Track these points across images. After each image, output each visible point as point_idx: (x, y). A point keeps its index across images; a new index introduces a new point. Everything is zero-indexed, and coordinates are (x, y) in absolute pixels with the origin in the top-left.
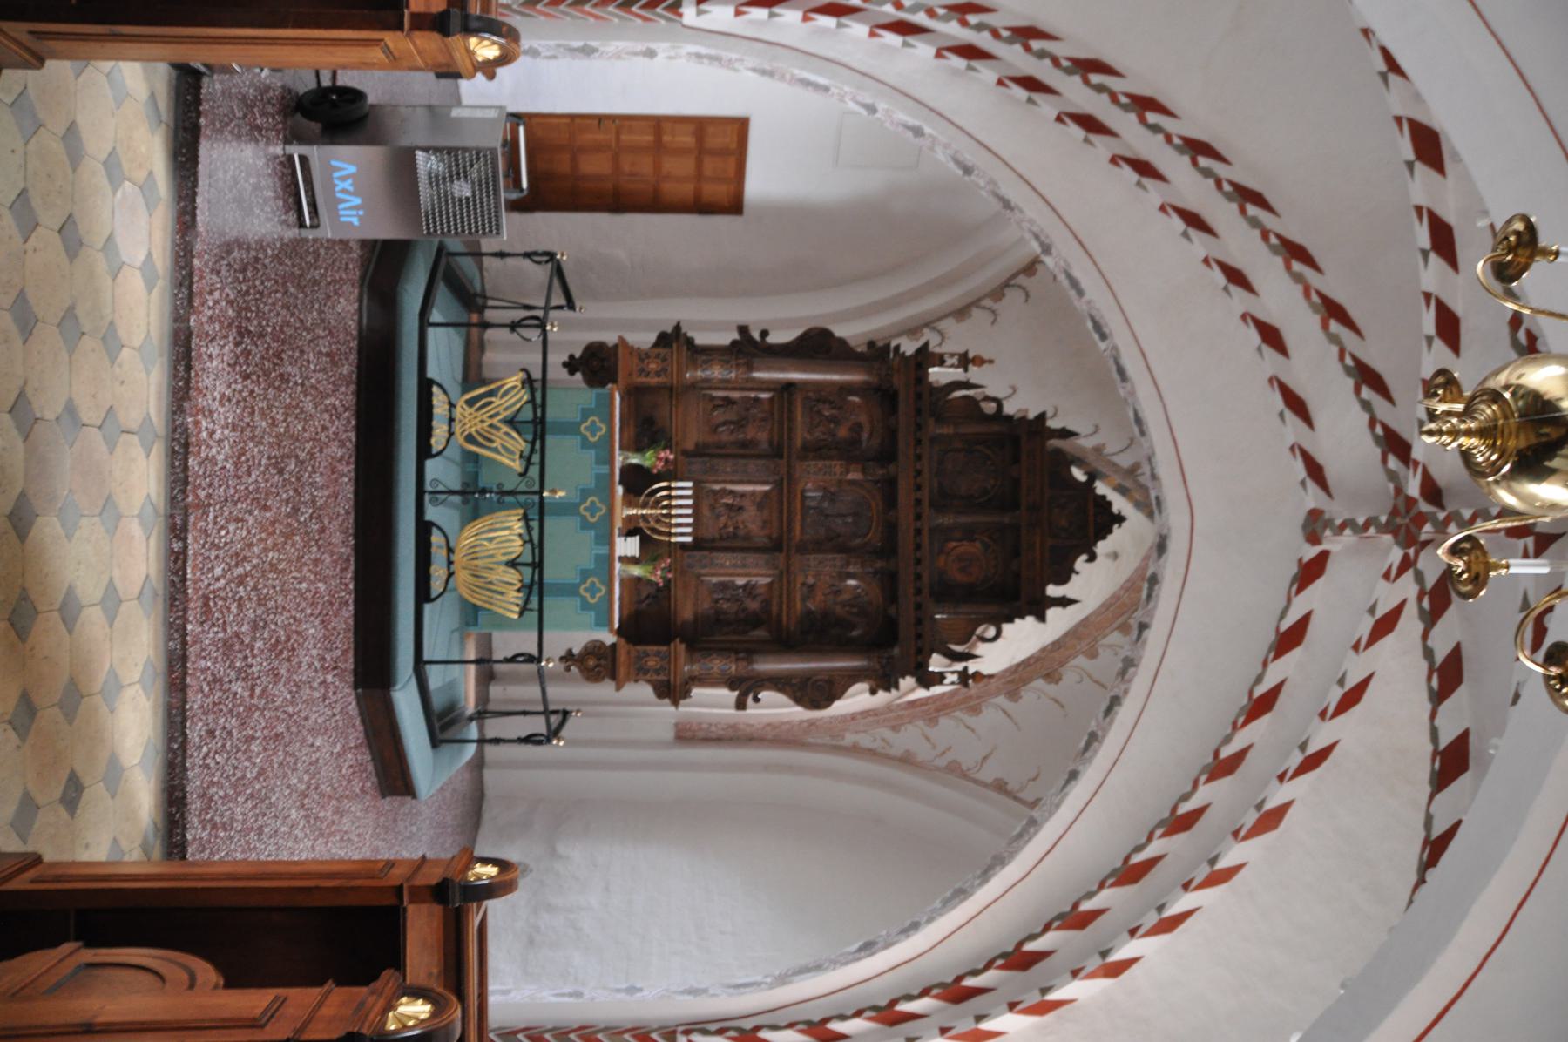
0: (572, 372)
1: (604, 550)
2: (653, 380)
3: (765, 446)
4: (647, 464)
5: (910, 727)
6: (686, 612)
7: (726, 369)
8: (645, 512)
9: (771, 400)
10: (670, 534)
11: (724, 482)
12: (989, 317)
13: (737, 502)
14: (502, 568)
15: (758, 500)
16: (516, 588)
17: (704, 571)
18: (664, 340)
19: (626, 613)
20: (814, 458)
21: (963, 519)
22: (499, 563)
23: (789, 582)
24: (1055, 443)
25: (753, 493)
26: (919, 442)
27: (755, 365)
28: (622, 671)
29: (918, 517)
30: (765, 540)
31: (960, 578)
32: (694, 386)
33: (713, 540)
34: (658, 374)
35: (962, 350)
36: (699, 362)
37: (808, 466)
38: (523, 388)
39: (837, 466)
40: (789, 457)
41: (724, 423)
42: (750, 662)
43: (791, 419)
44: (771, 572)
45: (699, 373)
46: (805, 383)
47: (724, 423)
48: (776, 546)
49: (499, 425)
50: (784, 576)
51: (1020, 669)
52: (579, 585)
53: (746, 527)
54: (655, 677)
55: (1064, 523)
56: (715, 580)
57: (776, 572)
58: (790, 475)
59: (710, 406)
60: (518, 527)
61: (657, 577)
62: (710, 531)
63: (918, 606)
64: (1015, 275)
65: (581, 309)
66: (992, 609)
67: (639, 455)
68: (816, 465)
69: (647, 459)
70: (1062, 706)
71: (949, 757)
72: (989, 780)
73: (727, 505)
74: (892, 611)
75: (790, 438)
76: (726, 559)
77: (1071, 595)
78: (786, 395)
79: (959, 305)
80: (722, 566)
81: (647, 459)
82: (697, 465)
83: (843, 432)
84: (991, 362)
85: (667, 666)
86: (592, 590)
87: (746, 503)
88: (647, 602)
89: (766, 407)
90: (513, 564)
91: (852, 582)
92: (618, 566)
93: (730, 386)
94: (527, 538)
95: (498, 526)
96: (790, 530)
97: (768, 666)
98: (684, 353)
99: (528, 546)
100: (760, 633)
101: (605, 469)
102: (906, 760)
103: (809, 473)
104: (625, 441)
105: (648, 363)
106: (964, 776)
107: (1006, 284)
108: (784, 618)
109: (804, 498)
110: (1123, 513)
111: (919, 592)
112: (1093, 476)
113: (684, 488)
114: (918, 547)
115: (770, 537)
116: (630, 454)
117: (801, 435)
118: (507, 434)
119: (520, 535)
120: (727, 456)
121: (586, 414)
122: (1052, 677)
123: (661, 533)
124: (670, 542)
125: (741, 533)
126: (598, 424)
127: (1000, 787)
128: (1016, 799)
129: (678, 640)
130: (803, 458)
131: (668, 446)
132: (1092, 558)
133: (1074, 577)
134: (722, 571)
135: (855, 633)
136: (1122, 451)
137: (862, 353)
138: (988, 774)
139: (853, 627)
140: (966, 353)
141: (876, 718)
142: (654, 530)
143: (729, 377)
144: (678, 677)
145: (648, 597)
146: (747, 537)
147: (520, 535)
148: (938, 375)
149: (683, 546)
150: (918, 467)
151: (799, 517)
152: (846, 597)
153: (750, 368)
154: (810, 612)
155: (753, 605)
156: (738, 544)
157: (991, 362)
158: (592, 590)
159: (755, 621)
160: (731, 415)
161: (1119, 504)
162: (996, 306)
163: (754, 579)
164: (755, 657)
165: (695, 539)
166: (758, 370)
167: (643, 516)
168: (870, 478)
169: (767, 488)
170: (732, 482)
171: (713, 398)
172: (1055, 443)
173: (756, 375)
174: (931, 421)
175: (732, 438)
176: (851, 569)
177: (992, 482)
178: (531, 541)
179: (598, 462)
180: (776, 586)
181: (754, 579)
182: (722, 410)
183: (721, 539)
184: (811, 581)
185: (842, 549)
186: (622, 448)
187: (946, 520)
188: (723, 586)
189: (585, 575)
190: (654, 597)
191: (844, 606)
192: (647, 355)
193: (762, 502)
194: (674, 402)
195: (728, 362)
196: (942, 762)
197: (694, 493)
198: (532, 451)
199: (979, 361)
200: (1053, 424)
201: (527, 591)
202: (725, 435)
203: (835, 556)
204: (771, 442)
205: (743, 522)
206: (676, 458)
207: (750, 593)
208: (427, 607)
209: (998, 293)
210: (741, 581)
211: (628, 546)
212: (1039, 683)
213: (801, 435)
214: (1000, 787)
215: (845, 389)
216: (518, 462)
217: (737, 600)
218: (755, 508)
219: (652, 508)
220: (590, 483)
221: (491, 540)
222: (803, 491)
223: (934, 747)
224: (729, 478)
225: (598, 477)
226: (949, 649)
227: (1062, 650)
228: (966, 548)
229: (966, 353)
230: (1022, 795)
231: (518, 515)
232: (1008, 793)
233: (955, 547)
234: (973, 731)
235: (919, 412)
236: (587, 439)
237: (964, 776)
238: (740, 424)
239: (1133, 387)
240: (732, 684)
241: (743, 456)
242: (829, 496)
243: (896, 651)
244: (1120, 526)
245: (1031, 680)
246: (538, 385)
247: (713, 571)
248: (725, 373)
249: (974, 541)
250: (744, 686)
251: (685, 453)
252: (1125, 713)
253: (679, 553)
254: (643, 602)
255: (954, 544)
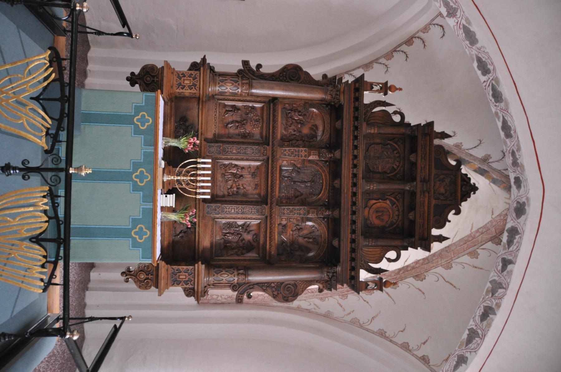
0: (133, 85)
1: (149, 206)
2: (187, 92)
3: (258, 136)
4: (181, 146)
5: (331, 299)
6: (205, 241)
7: (235, 86)
8: (179, 178)
9: (262, 108)
10: (196, 193)
11: (232, 159)
12: (383, 69)
13: (240, 172)
14: (27, 243)
15: (253, 171)
16: (41, 263)
17: (217, 216)
18: (194, 66)
19: (166, 243)
20: (288, 146)
21: (382, 187)
22: (23, 240)
23: (271, 224)
24: (437, 142)
25: (249, 167)
26: (356, 138)
27: (254, 85)
28: (162, 283)
29: (355, 185)
30: (256, 196)
31: (376, 222)
32: (212, 97)
33: (224, 196)
34: (190, 88)
35: (384, 82)
36: (218, 81)
37: (285, 150)
38: (50, 66)
39: (303, 151)
40: (273, 144)
41: (232, 122)
42: (246, 275)
43: (275, 121)
44: (259, 217)
45: (218, 89)
46: (284, 98)
47: (232, 122)
48: (263, 201)
49: (24, 101)
50: (268, 220)
51: (401, 272)
52: (131, 230)
53: (244, 188)
54: (185, 286)
55: (442, 190)
56: (224, 221)
57: (263, 217)
58: (273, 156)
59: (224, 110)
60: (43, 204)
61: (187, 221)
62: (222, 190)
63: (353, 241)
64: (400, 45)
65: (136, 36)
66: (397, 243)
67: (176, 141)
68: (289, 150)
69: (182, 143)
70: (423, 293)
71: (352, 316)
72: (375, 329)
73: (233, 174)
74: (335, 243)
75: (273, 132)
76: (231, 209)
77: (445, 235)
78: (272, 105)
79: (367, 61)
80: (230, 213)
81: (182, 143)
82: (214, 148)
83: (306, 131)
84: (400, 89)
85: (193, 279)
86: (140, 233)
87: (245, 173)
88: (180, 235)
89: (259, 113)
90: (37, 240)
91: (310, 223)
92: (159, 215)
93: (237, 98)
94: (51, 214)
95: (22, 202)
96: (272, 191)
97: (256, 278)
98: (208, 76)
99: (53, 221)
100: (252, 255)
101: (151, 149)
102: (327, 316)
103: (285, 155)
104: (168, 131)
105: (184, 80)
106: (361, 327)
107: (395, 50)
108: (268, 247)
109: (281, 170)
110: (477, 185)
111: (353, 232)
112: (460, 163)
113: (205, 163)
114: (354, 204)
115: (259, 195)
116: (170, 140)
117: (280, 131)
118: (33, 110)
119: (45, 212)
120: (233, 143)
121: (138, 109)
122: (419, 277)
123: (189, 193)
124: (196, 198)
125: (242, 191)
126: (147, 117)
127: (382, 334)
128: (391, 341)
129: (200, 263)
130: (282, 146)
131: (196, 135)
132: (458, 212)
133: (447, 223)
134: (228, 216)
135: (311, 254)
136: (475, 147)
137: (318, 81)
138: (375, 326)
139: (309, 250)
140: (387, 83)
141: (312, 294)
142: (184, 190)
143: (236, 91)
144: (200, 287)
145: (181, 232)
146: (245, 195)
147: (45, 212)
148: (368, 97)
149: (204, 200)
150: (355, 153)
151: (278, 182)
152: (305, 232)
153: (251, 86)
154: (283, 242)
155: (248, 237)
156: (239, 199)
157: (400, 89)
158: (140, 233)
159: (249, 247)
160: (236, 117)
161: (476, 179)
162: (387, 63)
163: (248, 221)
164: (250, 272)
165: (213, 195)
166: (256, 88)
167: (178, 180)
168: (323, 159)
169: (258, 163)
170: (237, 159)
171: (225, 106)
172: (437, 142)
173: (254, 91)
174: (364, 125)
175: (237, 131)
176: (310, 216)
177: (397, 164)
178: (56, 217)
179: (146, 144)
180: (263, 226)
181: (248, 221)
182: (231, 113)
183: (229, 195)
184: (284, 222)
185: (303, 203)
186: (164, 136)
187: (373, 187)
188: (230, 225)
189: (135, 222)
190: (185, 232)
191: (305, 238)
192: (184, 75)
193: (255, 173)
194: (200, 106)
195: (236, 82)
196: (348, 318)
197: (212, 166)
198: (59, 128)
199: (393, 89)
200: (438, 128)
201: (52, 266)
202: (232, 130)
203: (301, 207)
204: (261, 134)
205: (242, 185)
206: (201, 143)
207: (246, 230)
208: (404, 45)
209: (389, 55)
210: (240, 222)
211: (170, 201)
212: (411, 280)
213: (280, 131)
214: (382, 334)
215: (309, 103)
216: (44, 140)
217: (238, 234)
218: (250, 176)
219: (184, 176)
220: (140, 158)
221: (14, 216)
222: (280, 167)
223: (344, 310)
224: (234, 157)
225: (146, 154)
226: (369, 266)
227: (429, 264)
228: (381, 204)
229: (387, 83)
230: (394, 339)
231: (44, 191)
232: (386, 338)
233: (374, 204)
234: (367, 302)
235: (356, 118)
236: (139, 127)
237: (361, 327)
238: (242, 123)
239: (507, 104)
240: (234, 287)
241: (243, 143)
242: (297, 170)
243: (339, 269)
244: (474, 193)
245: (406, 278)
246: (66, 63)
247: (223, 216)
248: (235, 88)
249: (386, 200)
250: (241, 289)
251: (206, 140)
252: (498, 320)
253: (201, 204)
254: (178, 235)
255: (374, 201)
